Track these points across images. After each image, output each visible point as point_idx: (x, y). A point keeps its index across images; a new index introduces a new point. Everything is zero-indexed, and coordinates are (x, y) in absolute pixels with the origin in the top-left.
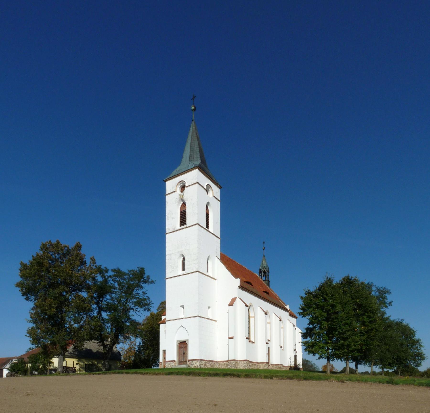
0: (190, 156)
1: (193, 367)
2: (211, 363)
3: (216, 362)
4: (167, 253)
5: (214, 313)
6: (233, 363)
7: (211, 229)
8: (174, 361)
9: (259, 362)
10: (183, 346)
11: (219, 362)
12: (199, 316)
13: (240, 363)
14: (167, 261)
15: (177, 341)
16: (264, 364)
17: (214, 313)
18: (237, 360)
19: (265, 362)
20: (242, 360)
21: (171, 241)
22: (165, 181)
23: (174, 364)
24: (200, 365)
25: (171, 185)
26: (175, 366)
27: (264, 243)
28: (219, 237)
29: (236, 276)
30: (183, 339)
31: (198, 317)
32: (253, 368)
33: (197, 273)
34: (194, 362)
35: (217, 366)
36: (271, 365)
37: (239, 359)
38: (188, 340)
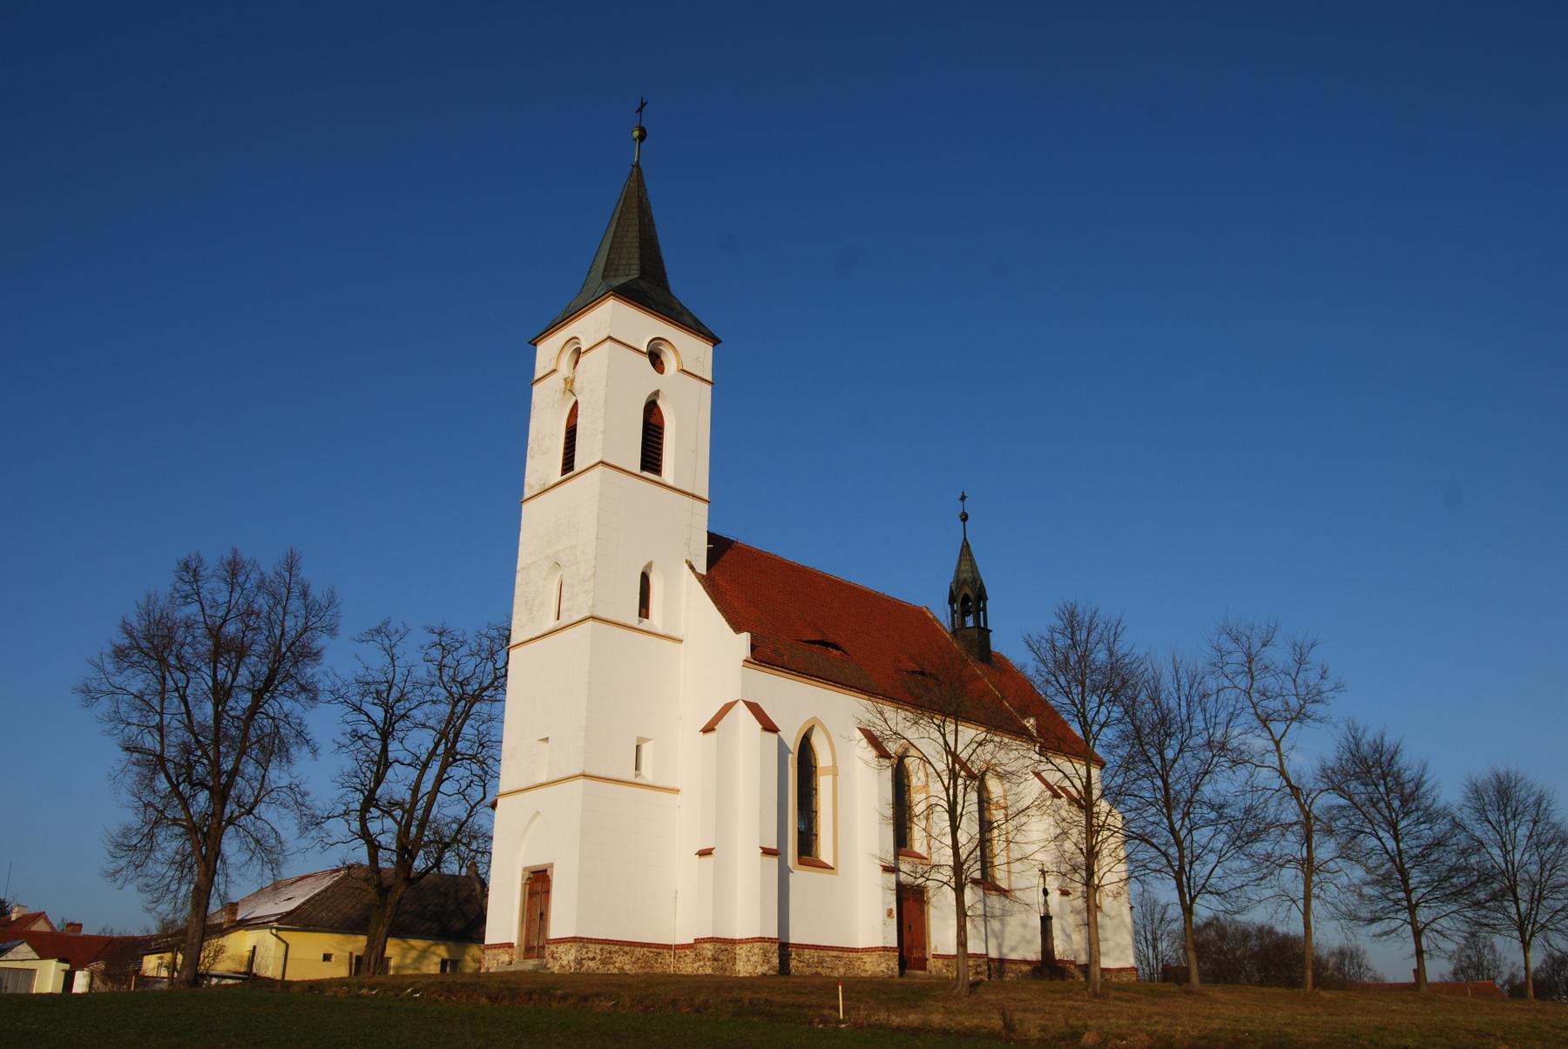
0: (608, 264)
1: (556, 969)
2: (639, 952)
3: (668, 947)
4: (521, 562)
5: (644, 764)
6: (708, 950)
7: (668, 474)
8: (510, 945)
9: (860, 946)
10: (538, 883)
11: (678, 947)
12: (585, 776)
13: (742, 951)
14: (518, 590)
15: (525, 869)
16: (875, 956)
17: (644, 764)
18: (733, 942)
19: (878, 942)
20: (746, 941)
21: (539, 524)
22: (534, 343)
23: (506, 958)
24: (579, 962)
25: (548, 352)
26: (510, 963)
27: (963, 498)
28: (706, 497)
29: (738, 628)
30: (537, 861)
31: (581, 781)
32: (824, 972)
33: (590, 623)
34: (562, 948)
35: (670, 965)
36: (936, 956)
37: (738, 937)
38: (551, 865)
